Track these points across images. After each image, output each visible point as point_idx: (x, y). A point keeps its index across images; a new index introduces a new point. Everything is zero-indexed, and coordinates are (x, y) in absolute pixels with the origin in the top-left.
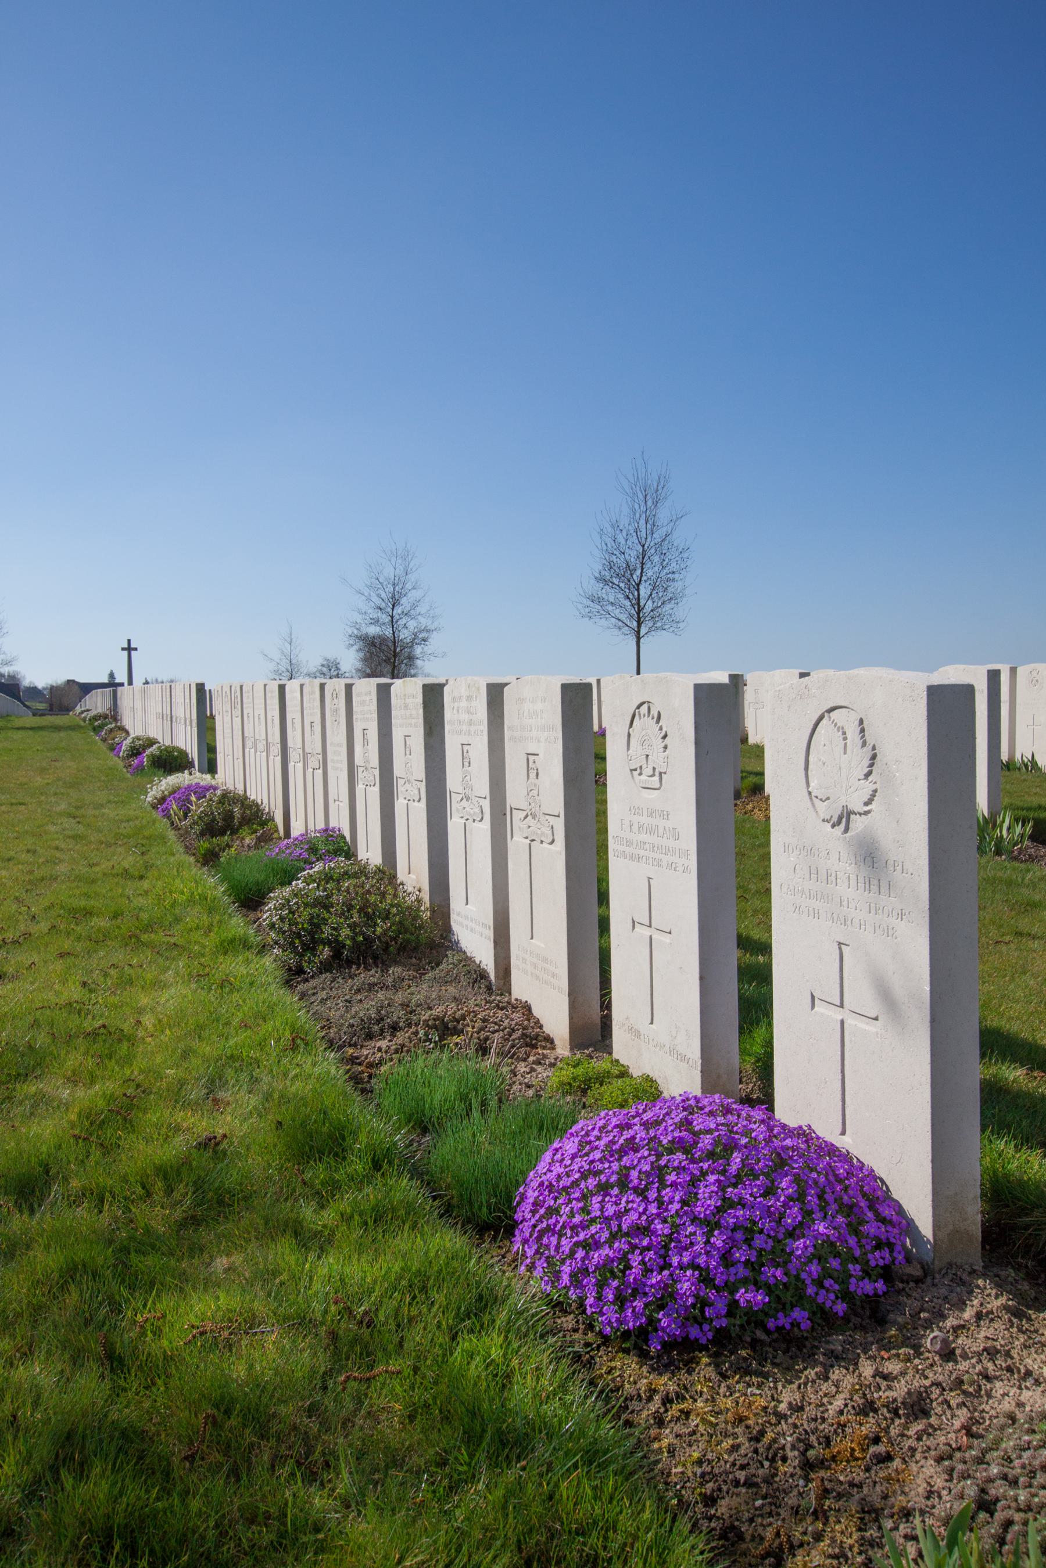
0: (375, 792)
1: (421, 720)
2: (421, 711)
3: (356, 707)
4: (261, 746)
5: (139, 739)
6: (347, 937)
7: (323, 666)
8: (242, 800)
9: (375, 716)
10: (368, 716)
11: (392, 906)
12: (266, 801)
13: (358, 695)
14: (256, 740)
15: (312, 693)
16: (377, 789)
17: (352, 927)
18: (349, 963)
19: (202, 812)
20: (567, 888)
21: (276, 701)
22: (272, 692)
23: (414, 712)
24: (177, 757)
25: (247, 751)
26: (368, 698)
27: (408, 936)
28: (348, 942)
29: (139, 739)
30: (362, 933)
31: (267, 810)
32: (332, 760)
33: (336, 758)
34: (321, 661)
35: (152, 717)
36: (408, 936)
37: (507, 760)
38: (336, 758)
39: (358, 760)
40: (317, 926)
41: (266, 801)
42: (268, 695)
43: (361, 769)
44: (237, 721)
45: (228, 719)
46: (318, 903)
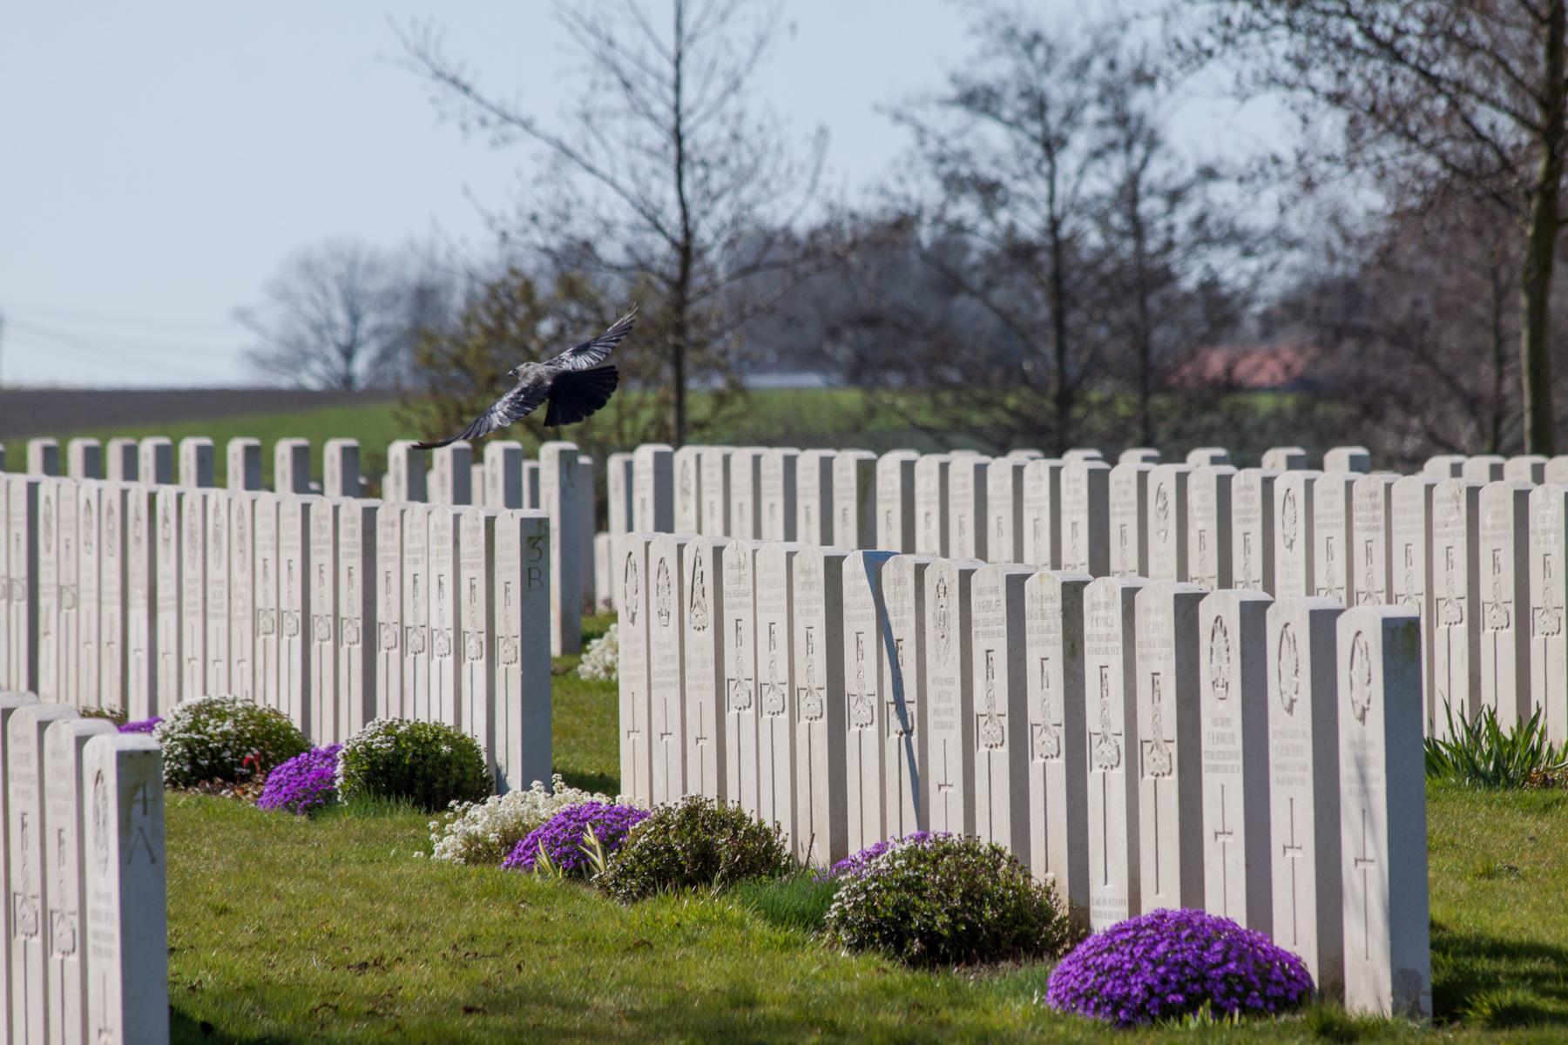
0: (1002, 754)
1: (1060, 635)
2: (1060, 621)
3: (976, 613)
4: (774, 699)
5: (222, 716)
6: (944, 925)
7: (978, 100)
8: (732, 822)
9: (1004, 627)
10: (994, 628)
11: (1007, 888)
12: (786, 828)
13: (980, 592)
14: (759, 687)
15: (900, 581)
16: (1005, 749)
17: (952, 913)
18: (945, 961)
19: (643, 847)
20: (1181, 820)
21: (819, 593)
22: (808, 572)
23: (1052, 622)
24: (448, 760)
25: (731, 716)
26: (994, 598)
27: (1026, 928)
28: (946, 932)
29: (222, 716)
30: (966, 921)
31: (788, 848)
32: (936, 711)
33: (942, 706)
34: (959, 49)
35: (613, 627)
36: (1026, 928)
37: (1309, 729)
38: (942, 706)
39: (979, 706)
40: (906, 917)
41: (786, 828)
42: (798, 579)
43: (982, 720)
44: (701, 643)
45: (665, 634)
46: (907, 885)
